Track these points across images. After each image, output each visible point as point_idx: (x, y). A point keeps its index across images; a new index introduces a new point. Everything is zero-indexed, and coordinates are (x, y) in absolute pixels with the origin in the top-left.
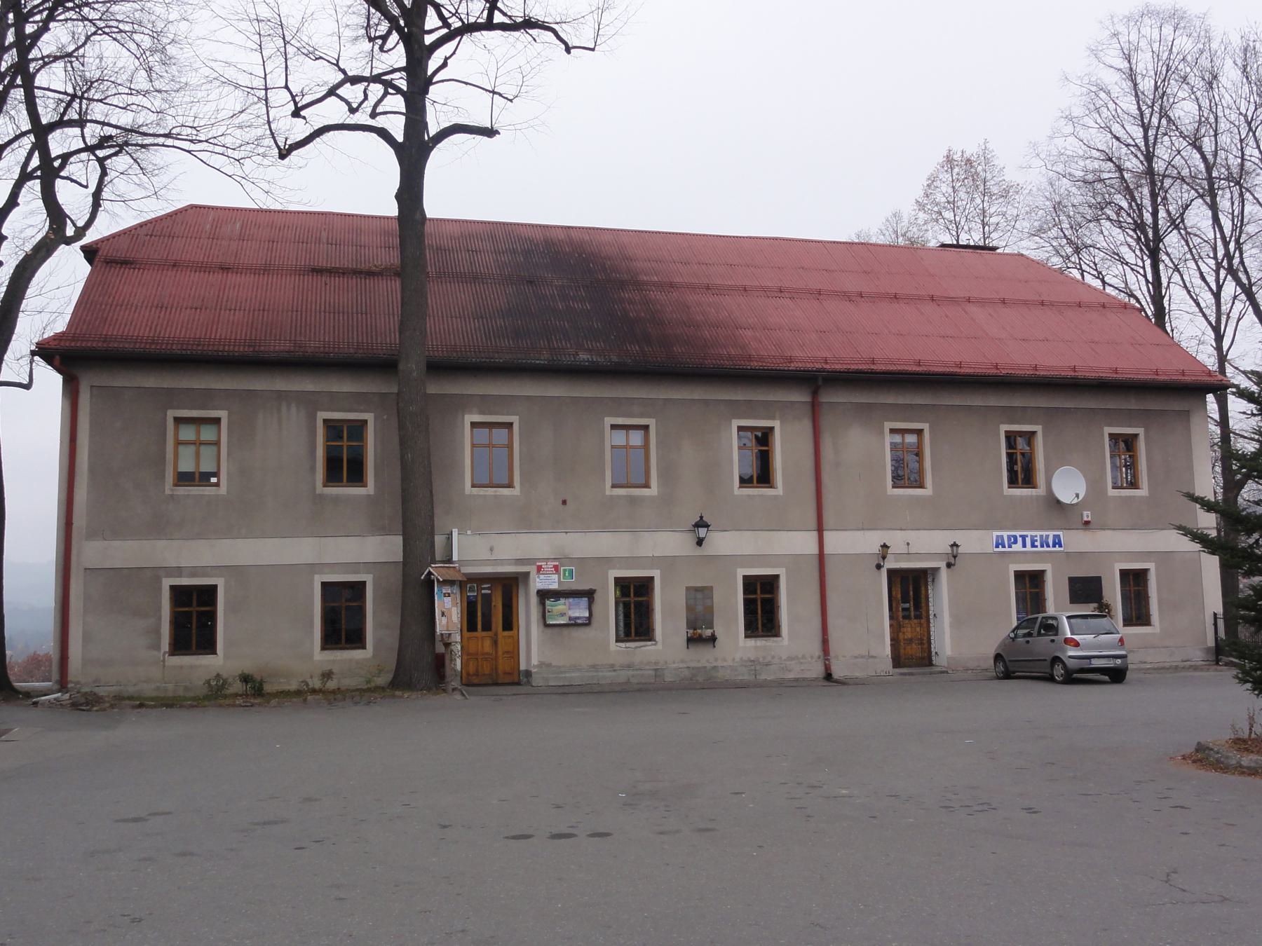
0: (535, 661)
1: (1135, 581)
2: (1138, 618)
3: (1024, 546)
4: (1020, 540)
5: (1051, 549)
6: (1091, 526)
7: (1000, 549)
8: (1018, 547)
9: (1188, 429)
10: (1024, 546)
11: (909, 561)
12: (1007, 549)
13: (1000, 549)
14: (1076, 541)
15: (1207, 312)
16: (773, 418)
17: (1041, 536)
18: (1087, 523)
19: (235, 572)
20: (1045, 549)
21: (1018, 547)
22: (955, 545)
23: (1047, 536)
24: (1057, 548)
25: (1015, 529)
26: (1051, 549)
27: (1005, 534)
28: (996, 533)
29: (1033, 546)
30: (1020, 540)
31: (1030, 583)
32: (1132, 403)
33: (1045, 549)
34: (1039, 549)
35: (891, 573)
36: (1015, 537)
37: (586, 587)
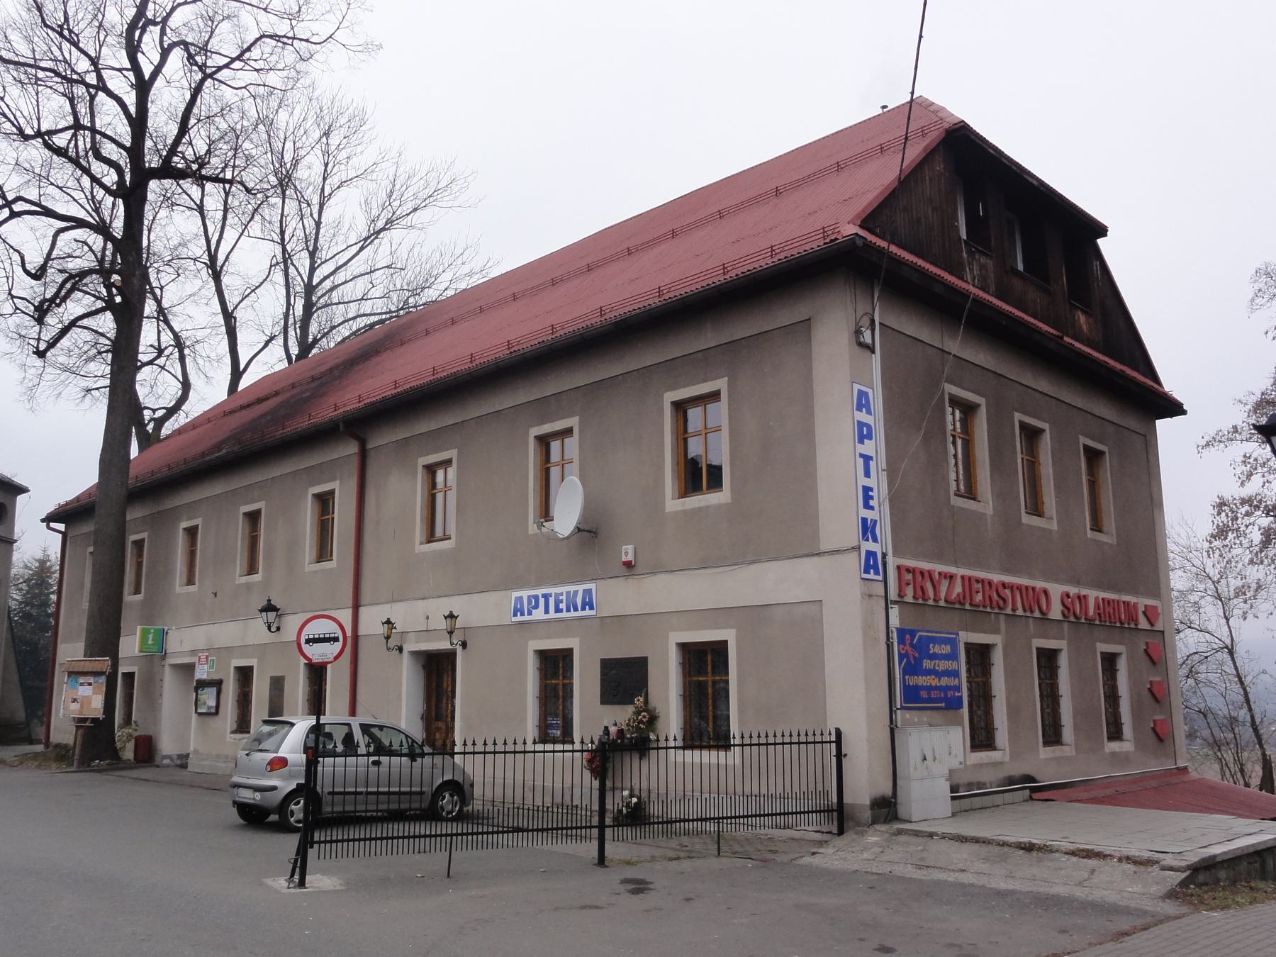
0: (192, 749)
1: (704, 661)
2: (717, 738)
3: (547, 611)
4: (542, 601)
5: (580, 613)
6: (638, 570)
7: (519, 618)
8: (538, 614)
9: (807, 358)
10: (547, 611)
11: (428, 640)
12: (526, 618)
13: (519, 618)
14: (618, 597)
15: (211, 229)
16: (333, 479)
17: (568, 593)
18: (628, 565)
19: (753, 616)
20: (573, 614)
21: (538, 614)
22: (451, 616)
23: (576, 592)
24: (588, 612)
25: (539, 584)
26: (580, 613)
27: (525, 594)
28: (515, 594)
29: (558, 610)
30: (542, 601)
31: (555, 665)
32: (708, 338)
33: (573, 614)
34: (565, 615)
35: (415, 654)
36: (536, 598)
37: (216, 677)
